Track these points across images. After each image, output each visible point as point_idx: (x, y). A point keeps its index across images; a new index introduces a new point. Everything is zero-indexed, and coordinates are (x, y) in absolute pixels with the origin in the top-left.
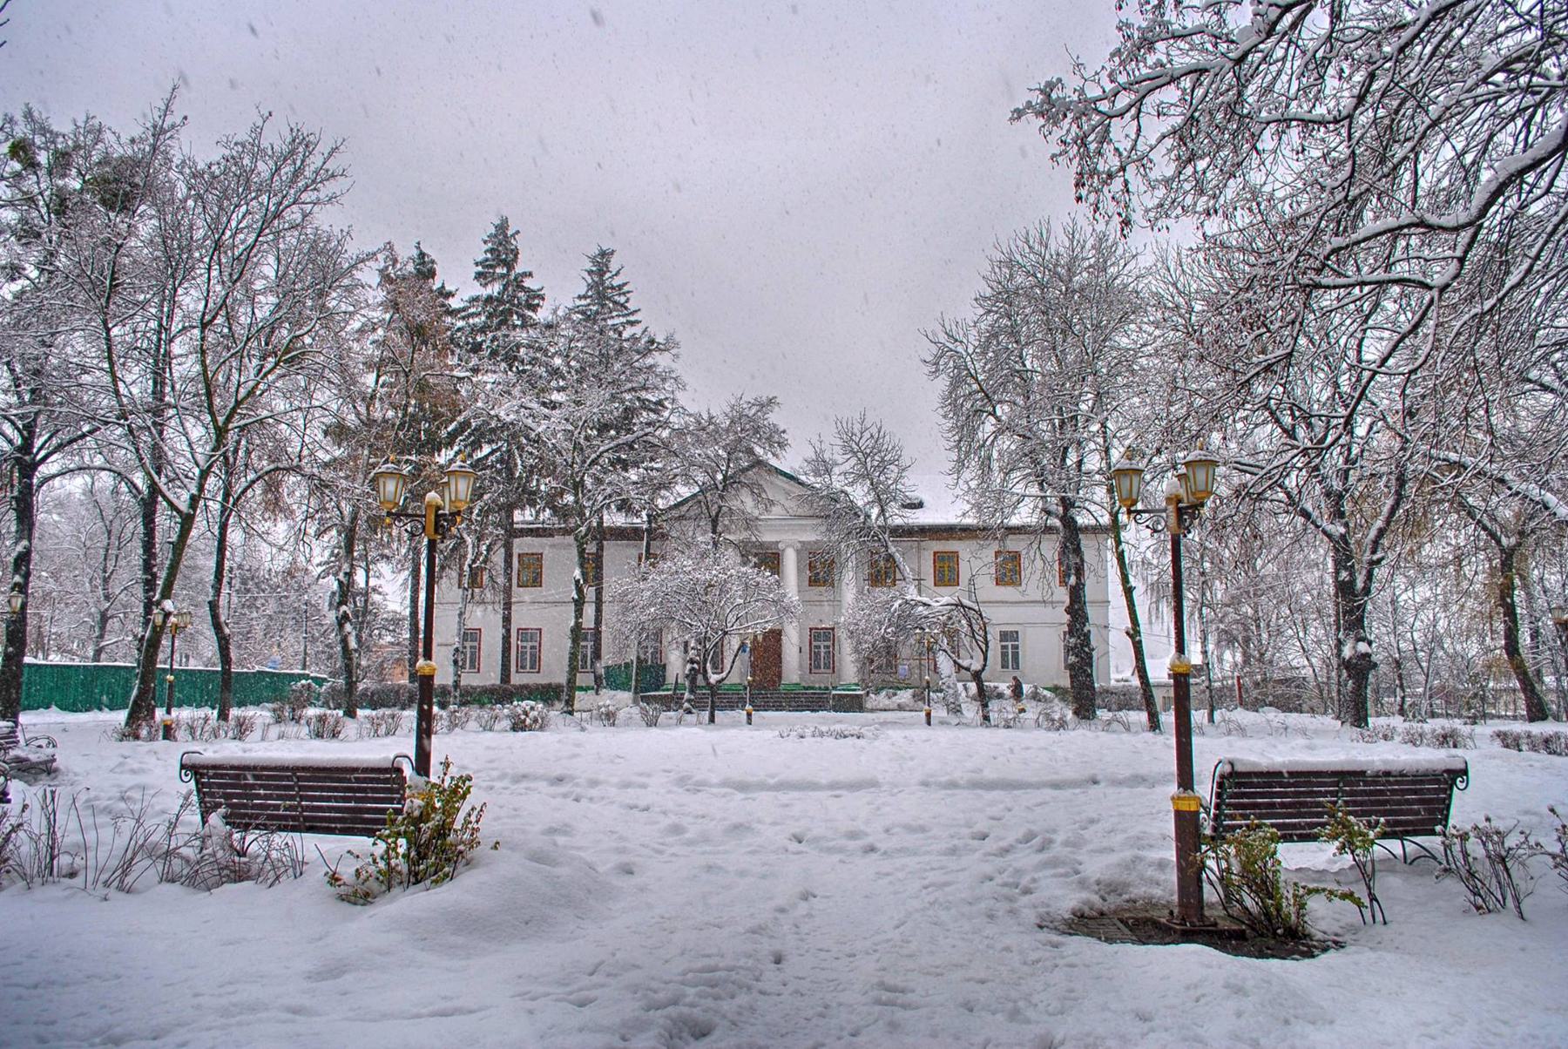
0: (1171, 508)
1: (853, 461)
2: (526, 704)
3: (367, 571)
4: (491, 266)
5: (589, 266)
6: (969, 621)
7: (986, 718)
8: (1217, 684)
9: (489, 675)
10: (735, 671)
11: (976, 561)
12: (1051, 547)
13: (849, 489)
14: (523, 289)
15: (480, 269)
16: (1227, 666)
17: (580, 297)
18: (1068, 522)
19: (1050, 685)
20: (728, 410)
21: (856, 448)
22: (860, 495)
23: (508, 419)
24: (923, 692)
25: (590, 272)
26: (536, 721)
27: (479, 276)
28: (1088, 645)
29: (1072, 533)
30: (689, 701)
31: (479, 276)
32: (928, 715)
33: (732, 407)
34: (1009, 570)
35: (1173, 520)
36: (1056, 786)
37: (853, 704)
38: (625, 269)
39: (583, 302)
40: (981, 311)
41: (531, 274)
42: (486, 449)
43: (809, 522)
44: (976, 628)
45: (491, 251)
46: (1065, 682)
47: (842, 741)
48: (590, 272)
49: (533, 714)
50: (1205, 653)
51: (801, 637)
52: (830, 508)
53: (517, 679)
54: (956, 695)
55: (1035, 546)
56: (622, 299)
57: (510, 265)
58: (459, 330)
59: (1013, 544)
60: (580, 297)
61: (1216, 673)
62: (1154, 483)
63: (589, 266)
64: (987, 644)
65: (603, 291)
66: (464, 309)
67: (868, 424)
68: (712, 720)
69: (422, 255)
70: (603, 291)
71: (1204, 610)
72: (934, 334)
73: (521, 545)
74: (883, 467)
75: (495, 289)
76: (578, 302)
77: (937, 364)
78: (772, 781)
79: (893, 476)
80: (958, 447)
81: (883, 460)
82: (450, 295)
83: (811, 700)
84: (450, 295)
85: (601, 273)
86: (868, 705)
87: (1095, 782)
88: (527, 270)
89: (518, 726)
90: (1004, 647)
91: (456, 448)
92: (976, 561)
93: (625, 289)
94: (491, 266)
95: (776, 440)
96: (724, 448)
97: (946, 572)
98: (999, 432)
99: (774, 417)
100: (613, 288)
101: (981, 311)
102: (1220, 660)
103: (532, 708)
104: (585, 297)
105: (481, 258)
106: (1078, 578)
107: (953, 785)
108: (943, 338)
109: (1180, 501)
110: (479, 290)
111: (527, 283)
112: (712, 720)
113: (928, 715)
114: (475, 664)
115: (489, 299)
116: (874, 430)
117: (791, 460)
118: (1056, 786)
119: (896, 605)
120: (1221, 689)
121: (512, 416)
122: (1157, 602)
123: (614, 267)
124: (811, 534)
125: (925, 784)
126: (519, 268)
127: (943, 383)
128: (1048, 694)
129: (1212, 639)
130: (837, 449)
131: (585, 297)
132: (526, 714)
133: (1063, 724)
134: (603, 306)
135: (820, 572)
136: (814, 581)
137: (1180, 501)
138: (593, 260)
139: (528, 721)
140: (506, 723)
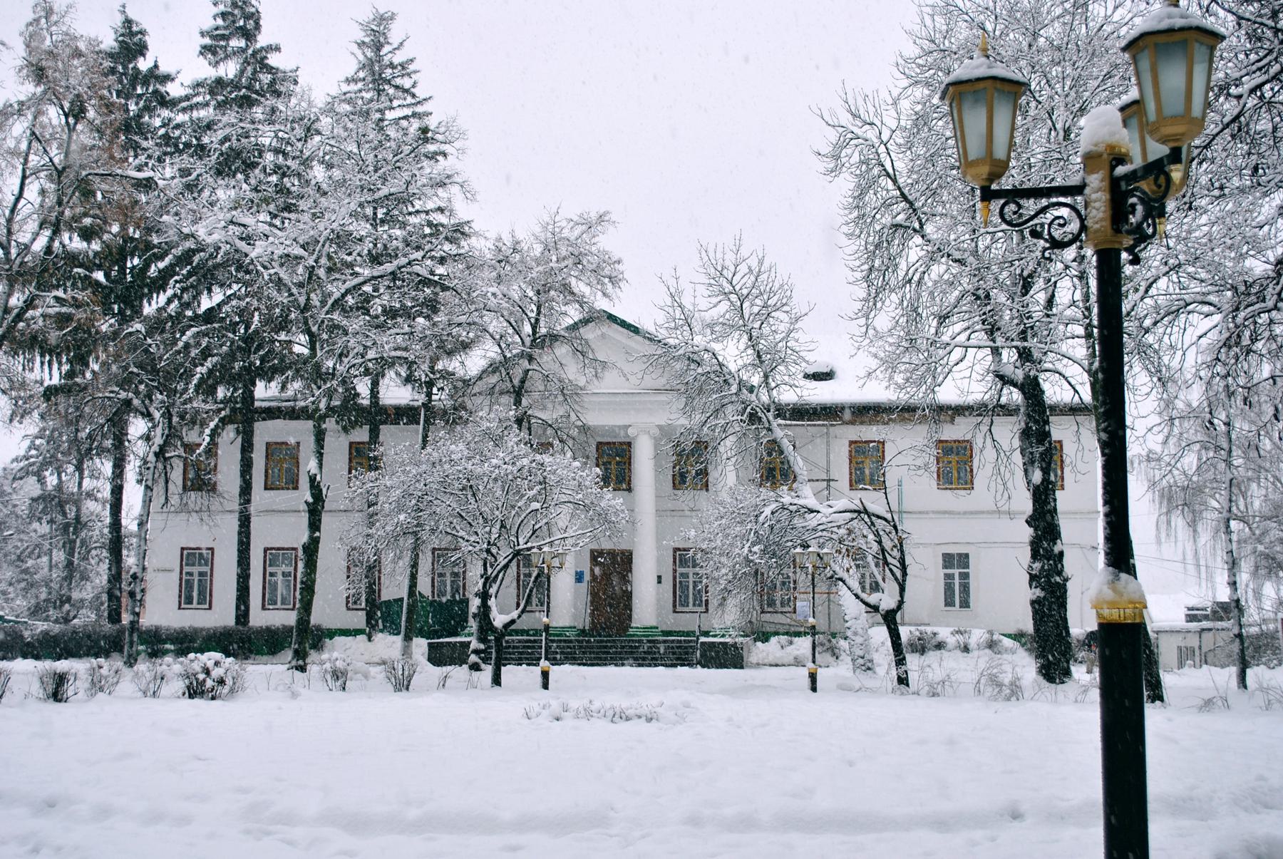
0: (1096, 181)
1: (724, 306)
2: (210, 658)
3: (79, 468)
4: (223, 37)
5: (360, 35)
6: (877, 534)
7: (903, 681)
8: (1254, 630)
9: (221, 615)
10: (567, 605)
11: (907, 450)
12: (1008, 432)
13: (716, 347)
14: (270, 69)
15: (207, 41)
16: (1268, 605)
17: (348, 81)
18: (1032, 389)
19: (1012, 631)
20: (537, 229)
21: (728, 288)
22: (733, 353)
23: (209, 240)
24: (826, 640)
25: (361, 45)
26: (221, 682)
27: (206, 50)
28: (1060, 573)
29: (1037, 412)
30: (476, 652)
31: (206, 50)
32: (813, 677)
33: (545, 228)
34: (955, 466)
35: (1099, 211)
36: (942, 824)
37: (725, 657)
38: (412, 41)
39: (353, 87)
40: (905, 83)
41: (278, 49)
42: (218, 296)
43: (663, 398)
44: (887, 544)
45: (224, 15)
46: (1029, 627)
47: (623, 726)
48: (361, 45)
49: (217, 672)
50: (1233, 584)
51: (659, 561)
52: (700, 380)
53: (259, 618)
54: (865, 644)
55: (984, 428)
56: (407, 83)
57: (249, 35)
58: (178, 126)
59: (955, 431)
60: (348, 81)
61: (1252, 615)
62: (1160, 329)
63: (360, 35)
64: (905, 574)
65: (380, 73)
66: (187, 98)
67: (744, 252)
68: (497, 680)
69: (128, 22)
70: (380, 73)
71: (1233, 524)
72: (833, 113)
73: (265, 432)
74: (766, 314)
75: (230, 69)
76: (345, 88)
77: (837, 157)
78: (413, 813)
79: (783, 327)
80: (867, 278)
81: (765, 306)
82: (167, 78)
83: (680, 651)
84: (167, 78)
85: (378, 47)
86: (753, 659)
87: (1016, 816)
88: (273, 42)
89: (195, 691)
90: (948, 576)
91: (170, 292)
92: (907, 450)
93: (412, 67)
94: (223, 37)
95: (607, 273)
96: (531, 283)
97: (866, 466)
98: (932, 258)
99: (607, 242)
100: (392, 66)
101: (905, 83)
102: (1258, 595)
103: (217, 664)
104: (354, 80)
105: (209, 24)
106: (1046, 471)
107: (746, 823)
108: (845, 119)
109: (1120, 159)
110: (205, 71)
111: (273, 60)
112: (497, 680)
113: (813, 677)
114: (206, 599)
115: (219, 82)
116: (754, 265)
117: (637, 302)
118: (942, 824)
119: (768, 511)
120: (1258, 637)
121: (216, 237)
122: (1168, 512)
123: (395, 36)
124: (672, 415)
125: (694, 821)
126: (262, 40)
127: (846, 183)
128: (1008, 642)
129: (1246, 568)
130: (702, 290)
131: (354, 80)
132: (207, 672)
133: (1015, 691)
134: (379, 92)
135: (689, 467)
136: (679, 481)
137: (1120, 159)
138: (365, 27)
139: (209, 683)
140: (180, 685)
